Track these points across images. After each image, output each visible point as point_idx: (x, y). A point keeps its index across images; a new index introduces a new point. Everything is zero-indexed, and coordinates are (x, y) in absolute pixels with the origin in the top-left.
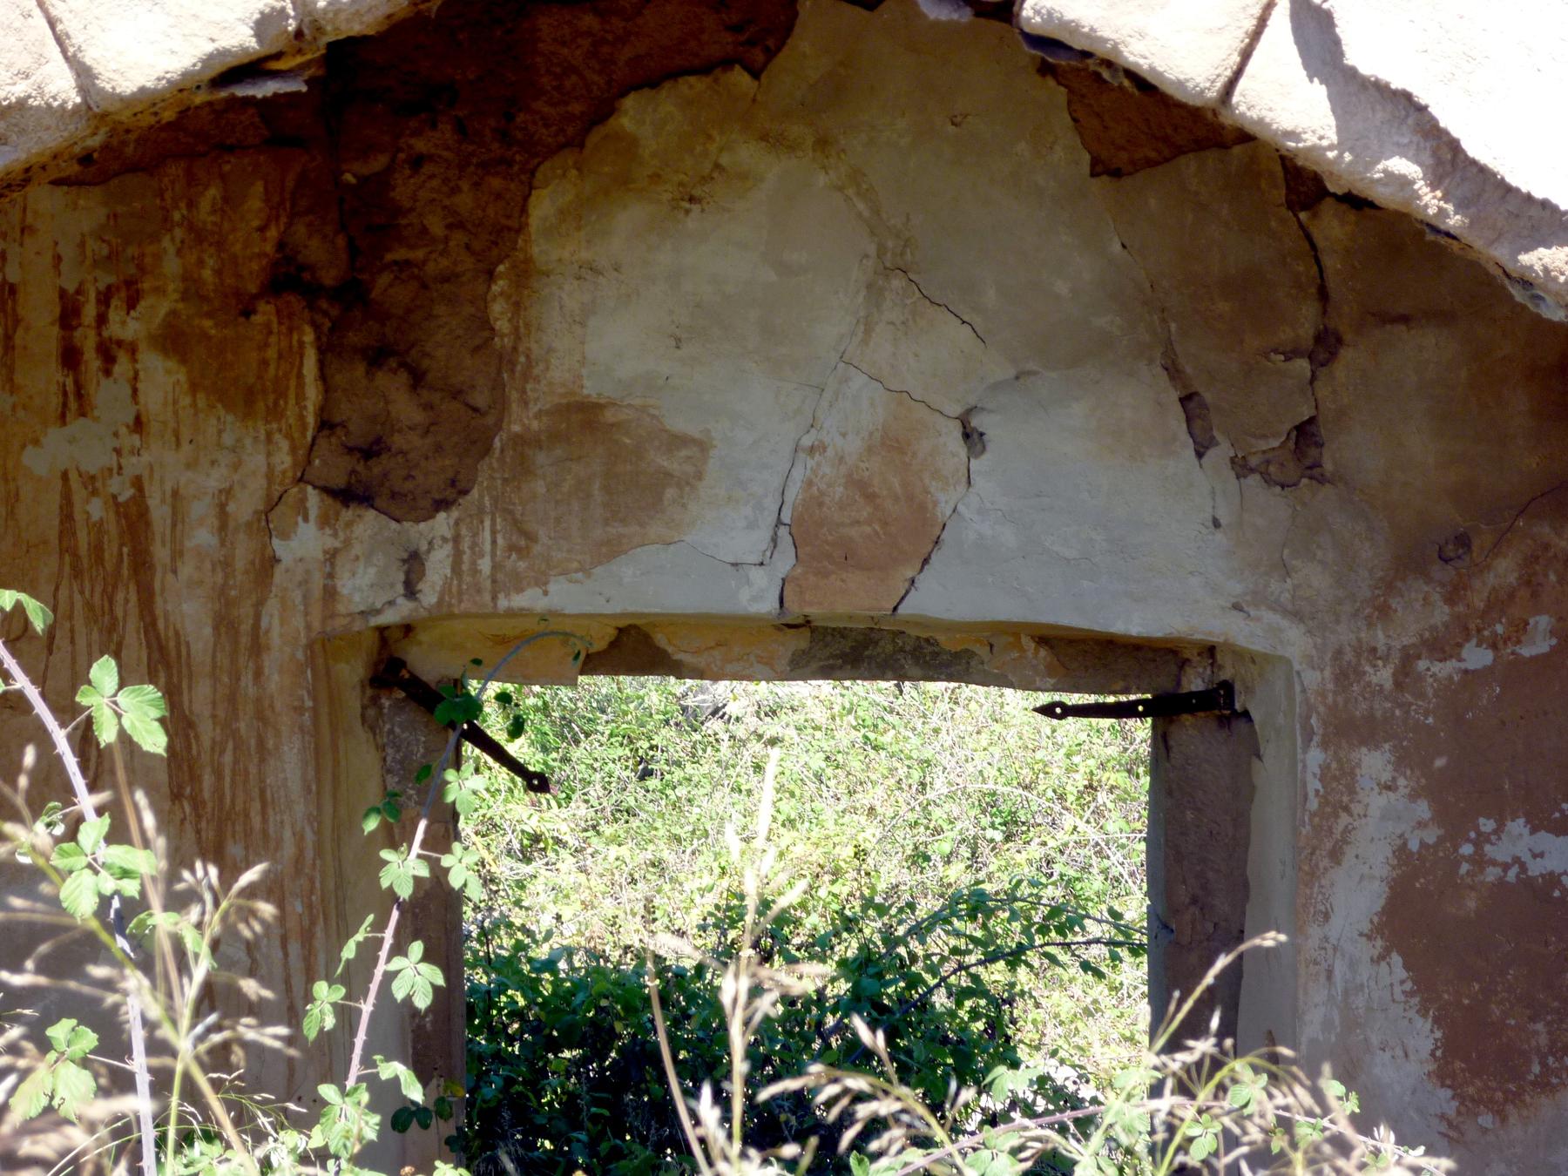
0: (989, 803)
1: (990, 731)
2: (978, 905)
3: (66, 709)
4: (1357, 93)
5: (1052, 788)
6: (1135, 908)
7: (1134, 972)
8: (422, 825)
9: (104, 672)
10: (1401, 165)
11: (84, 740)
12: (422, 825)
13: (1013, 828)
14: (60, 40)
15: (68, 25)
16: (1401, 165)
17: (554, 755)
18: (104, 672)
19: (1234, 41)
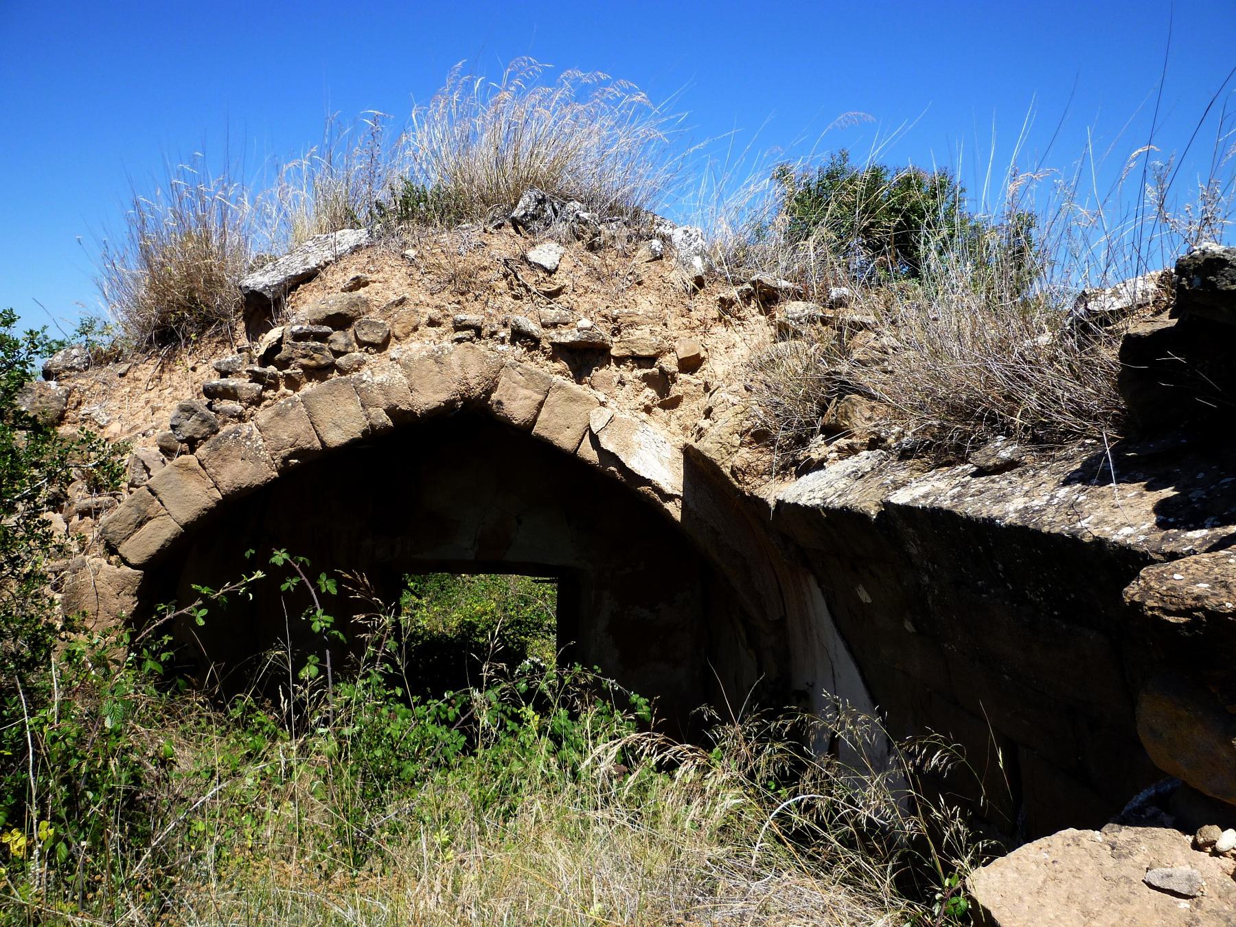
0: (521, 597)
1: (518, 584)
2: (519, 622)
3: (315, 585)
4: (603, 453)
5: (535, 596)
6: (554, 622)
7: (553, 637)
8: (328, 652)
9: (323, 577)
10: (612, 468)
11: (318, 591)
12: (328, 652)
13: (527, 603)
14: (318, 435)
15: (320, 432)
16: (612, 468)
17: (90, 858)
18: (323, 577)
19: (576, 441)
